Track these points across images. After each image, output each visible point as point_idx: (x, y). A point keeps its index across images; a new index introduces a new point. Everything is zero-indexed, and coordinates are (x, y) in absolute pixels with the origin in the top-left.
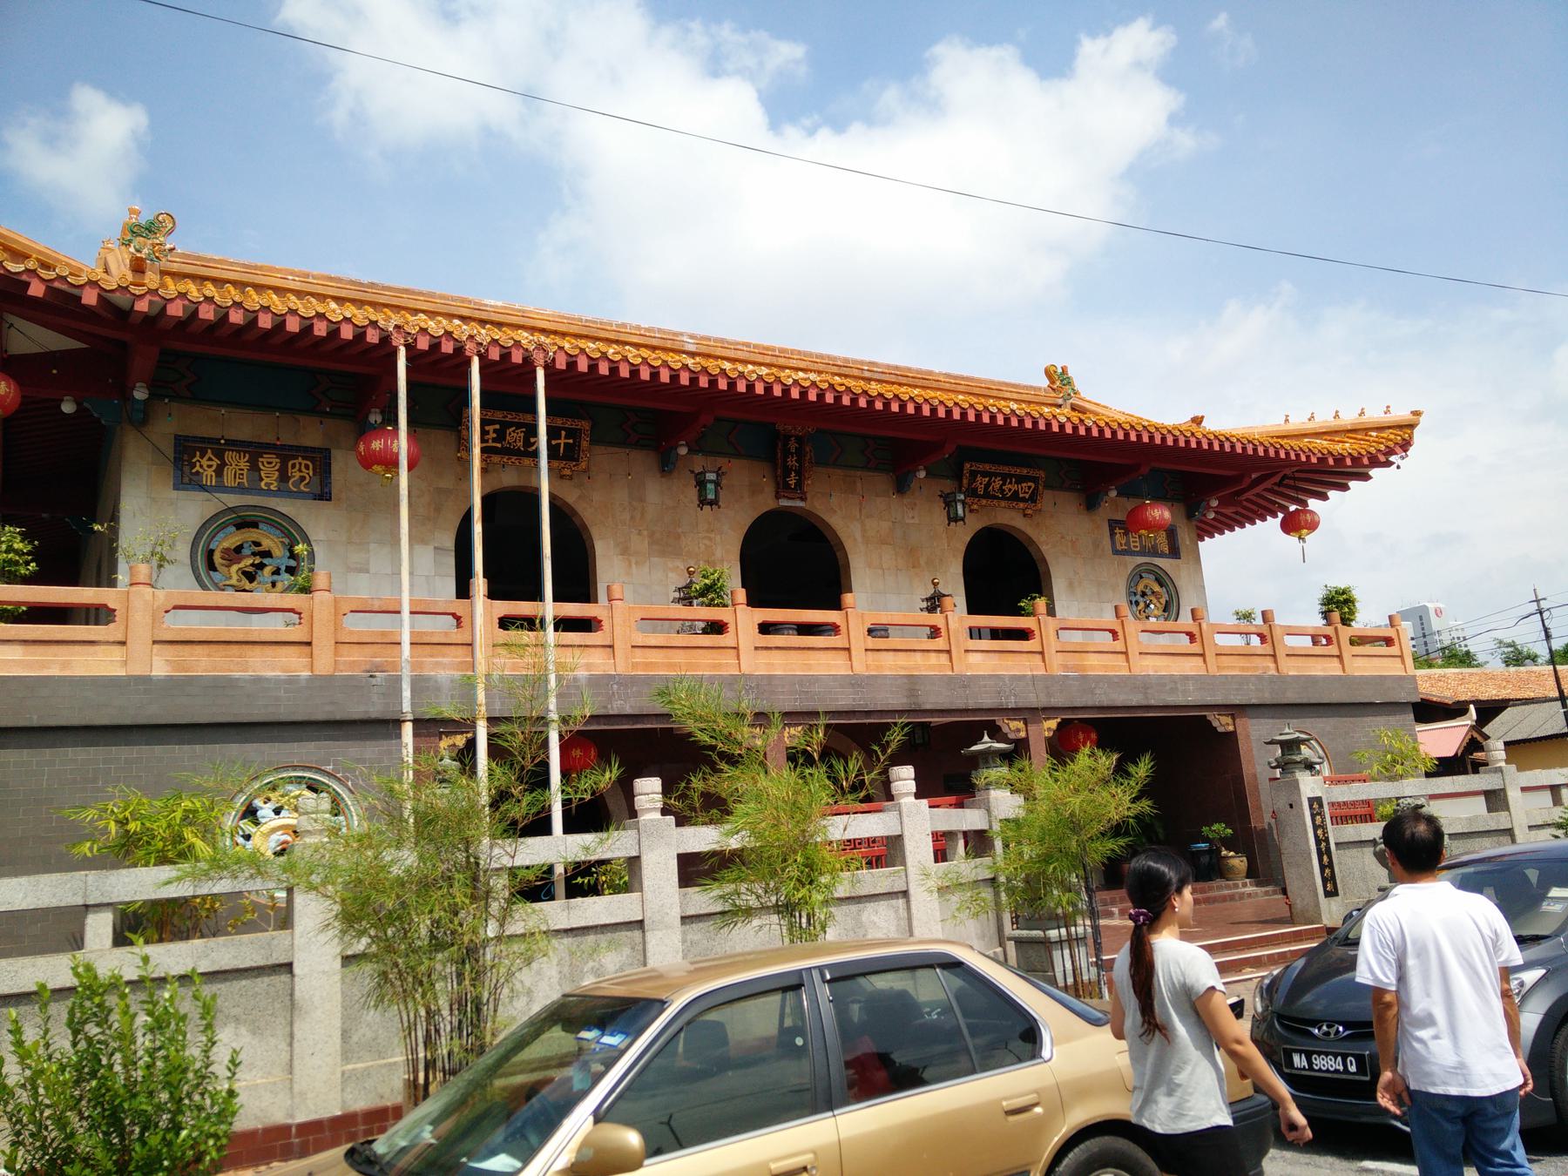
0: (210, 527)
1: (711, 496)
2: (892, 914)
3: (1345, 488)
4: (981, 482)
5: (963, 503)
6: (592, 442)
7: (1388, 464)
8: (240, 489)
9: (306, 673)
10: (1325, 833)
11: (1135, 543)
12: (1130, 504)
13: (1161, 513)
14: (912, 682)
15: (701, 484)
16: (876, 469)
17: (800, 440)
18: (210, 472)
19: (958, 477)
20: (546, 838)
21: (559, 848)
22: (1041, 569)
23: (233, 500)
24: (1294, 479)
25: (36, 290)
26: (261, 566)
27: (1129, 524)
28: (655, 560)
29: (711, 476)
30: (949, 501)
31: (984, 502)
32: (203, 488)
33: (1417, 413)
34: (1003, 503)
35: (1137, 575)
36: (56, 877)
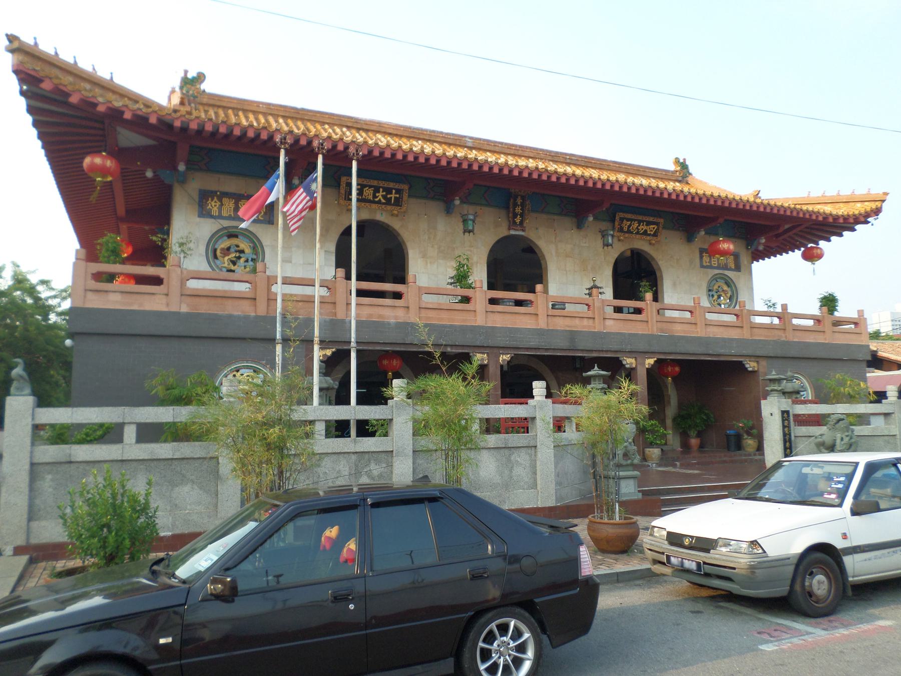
0: (215, 237)
1: (471, 228)
2: (528, 457)
3: (841, 235)
4: (626, 224)
5: (613, 236)
6: (409, 196)
7: (868, 222)
8: (229, 218)
9: (253, 314)
10: (789, 430)
11: (714, 262)
12: (712, 239)
13: (727, 246)
14: (572, 335)
15: (465, 221)
16: (565, 215)
17: (523, 198)
18: (215, 209)
19: (613, 220)
20: (345, 407)
21: (353, 411)
22: (658, 274)
23: (226, 223)
24: (812, 229)
25: (128, 116)
26: (239, 258)
27: (712, 251)
28: (441, 261)
29: (471, 217)
30: (604, 235)
31: (627, 235)
32: (212, 217)
33: (886, 194)
34: (638, 236)
35: (715, 278)
36: (110, 408)
